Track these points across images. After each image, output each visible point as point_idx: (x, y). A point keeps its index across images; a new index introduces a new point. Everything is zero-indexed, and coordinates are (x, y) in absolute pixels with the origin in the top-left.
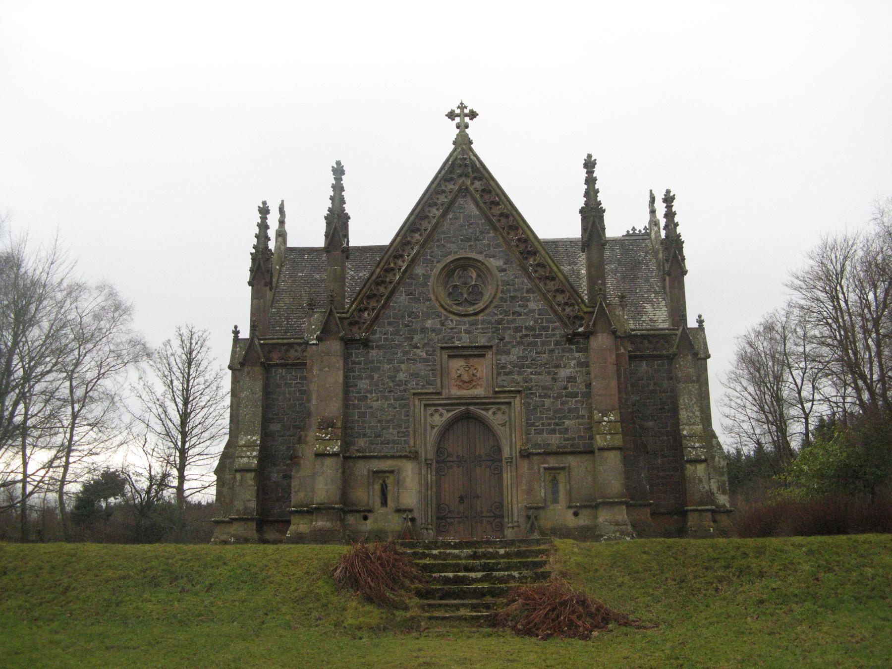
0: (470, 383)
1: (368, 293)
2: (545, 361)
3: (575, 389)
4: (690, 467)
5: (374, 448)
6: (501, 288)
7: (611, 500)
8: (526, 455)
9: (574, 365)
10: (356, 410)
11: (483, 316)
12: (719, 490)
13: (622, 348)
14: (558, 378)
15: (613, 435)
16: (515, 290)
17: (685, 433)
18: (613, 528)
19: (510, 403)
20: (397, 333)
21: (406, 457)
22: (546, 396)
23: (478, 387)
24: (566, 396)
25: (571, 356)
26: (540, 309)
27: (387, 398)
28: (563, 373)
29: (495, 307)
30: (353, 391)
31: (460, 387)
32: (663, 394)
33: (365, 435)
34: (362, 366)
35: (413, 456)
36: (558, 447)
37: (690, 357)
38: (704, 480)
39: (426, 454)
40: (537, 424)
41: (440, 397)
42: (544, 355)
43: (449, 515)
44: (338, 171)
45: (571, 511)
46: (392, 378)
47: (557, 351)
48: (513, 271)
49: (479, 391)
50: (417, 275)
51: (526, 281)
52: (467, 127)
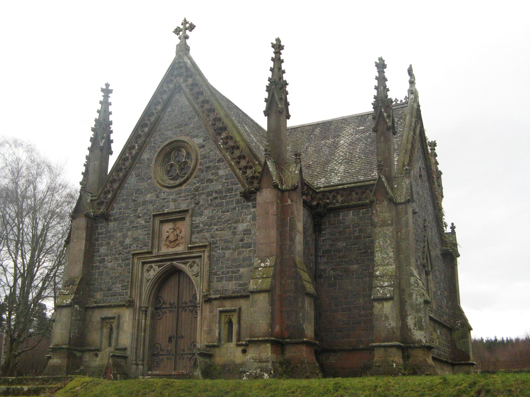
0: (175, 242)
1: (111, 179)
2: (228, 218)
3: (250, 241)
4: (378, 305)
5: (107, 299)
6: (200, 161)
7: (256, 339)
8: (208, 300)
9: (250, 219)
10: (97, 271)
11: (185, 186)
12: (415, 326)
13: (289, 200)
14: (237, 232)
15: (264, 279)
16: (210, 162)
17: (378, 273)
18: (256, 365)
19: (200, 257)
20: (127, 208)
21: (124, 306)
22: (227, 248)
23: (181, 245)
24: (242, 247)
25: (248, 211)
26: (226, 175)
27: (117, 259)
28: (241, 227)
29: (195, 177)
30: (96, 256)
31: (168, 247)
32: (367, 239)
33: (101, 290)
34: (103, 236)
35: (130, 304)
36: (233, 293)
37: (386, 203)
38: (390, 318)
39: (140, 303)
40: (219, 273)
41: (152, 255)
42: (228, 213)
43: (161, 353)
44: (107, 91)
45: (240, 349)
46: (122, 243)
47: (237, 209)
48: (210, 145)
49: (180, 249)
50: (143, 160)
51: (218, 153)
52: (187, 37)
